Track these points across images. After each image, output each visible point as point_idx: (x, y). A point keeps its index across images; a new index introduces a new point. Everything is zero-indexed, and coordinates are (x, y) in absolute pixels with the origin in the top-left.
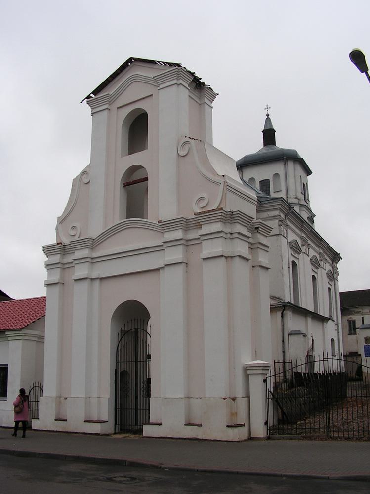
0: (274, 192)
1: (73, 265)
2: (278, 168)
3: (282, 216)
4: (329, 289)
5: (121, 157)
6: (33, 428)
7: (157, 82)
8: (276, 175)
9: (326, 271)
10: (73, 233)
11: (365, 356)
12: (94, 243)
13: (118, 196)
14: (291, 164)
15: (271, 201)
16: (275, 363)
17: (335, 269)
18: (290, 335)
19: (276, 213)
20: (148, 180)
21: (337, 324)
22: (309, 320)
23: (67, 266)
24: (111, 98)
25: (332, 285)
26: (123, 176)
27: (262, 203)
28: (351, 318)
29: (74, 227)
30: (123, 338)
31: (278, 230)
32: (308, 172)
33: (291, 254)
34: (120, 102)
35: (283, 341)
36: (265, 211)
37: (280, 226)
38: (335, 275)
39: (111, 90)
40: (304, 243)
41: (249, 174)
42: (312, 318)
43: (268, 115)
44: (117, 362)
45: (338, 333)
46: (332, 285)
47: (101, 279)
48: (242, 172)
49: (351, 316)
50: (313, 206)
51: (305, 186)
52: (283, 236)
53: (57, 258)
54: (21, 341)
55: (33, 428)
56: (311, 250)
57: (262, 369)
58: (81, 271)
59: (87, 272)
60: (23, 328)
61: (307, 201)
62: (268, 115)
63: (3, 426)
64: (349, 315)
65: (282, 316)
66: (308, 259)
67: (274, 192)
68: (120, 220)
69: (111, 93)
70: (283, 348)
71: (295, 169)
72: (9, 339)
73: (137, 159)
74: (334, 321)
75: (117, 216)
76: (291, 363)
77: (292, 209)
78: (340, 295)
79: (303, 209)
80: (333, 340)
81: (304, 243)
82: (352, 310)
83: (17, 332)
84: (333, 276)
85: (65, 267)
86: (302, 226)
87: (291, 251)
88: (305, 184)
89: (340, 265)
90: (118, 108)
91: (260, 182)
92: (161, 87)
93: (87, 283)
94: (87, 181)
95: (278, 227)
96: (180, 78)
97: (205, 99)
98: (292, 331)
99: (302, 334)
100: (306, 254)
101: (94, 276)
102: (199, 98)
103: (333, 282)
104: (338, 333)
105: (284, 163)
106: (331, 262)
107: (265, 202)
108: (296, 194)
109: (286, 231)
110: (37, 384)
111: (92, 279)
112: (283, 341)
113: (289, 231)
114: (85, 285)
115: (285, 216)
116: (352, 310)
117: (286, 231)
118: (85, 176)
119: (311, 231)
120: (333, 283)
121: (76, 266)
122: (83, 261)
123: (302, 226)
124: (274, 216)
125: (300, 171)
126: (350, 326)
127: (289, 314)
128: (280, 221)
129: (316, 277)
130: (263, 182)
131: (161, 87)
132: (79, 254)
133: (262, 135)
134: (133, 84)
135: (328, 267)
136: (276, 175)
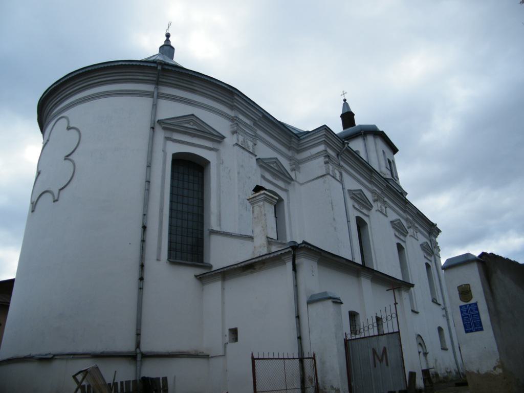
9: (409, 234)
11: (467, 332)
14: (370, 139)
16: (253, 359)
17: (433, 242)
18: (310, 302)
19: (322, 148)
21: (444, 308)
25: (431, 261)
27: (301, 138)
32: (394, 150)
33: (354, 206)
35: (298, 317)
37: (326, 163)
38: (435, 251)
40: (376, 198)
43: (345, 100)
45: (448, 320)
46: (431, 261)
52: (333, 177)
56: (388, 209)
62: (345, 100)
65: (295, 269)
66: (386, 222)
74: (439, 305)
77: (346, 146)
80: (440, 330)
84: (431, 250)
86: (371, 177)
99: (330, 298)
103: (433, 257)
104: (448, 320)
106: (427, 235)
112: (298, 317)
113: (344, 174)
119: (387, 186)
120: (432, 259)
124: (317, 153)
127: (307, 265)
129: (404, 247)
133: (340, 120)
135: (422, 239)
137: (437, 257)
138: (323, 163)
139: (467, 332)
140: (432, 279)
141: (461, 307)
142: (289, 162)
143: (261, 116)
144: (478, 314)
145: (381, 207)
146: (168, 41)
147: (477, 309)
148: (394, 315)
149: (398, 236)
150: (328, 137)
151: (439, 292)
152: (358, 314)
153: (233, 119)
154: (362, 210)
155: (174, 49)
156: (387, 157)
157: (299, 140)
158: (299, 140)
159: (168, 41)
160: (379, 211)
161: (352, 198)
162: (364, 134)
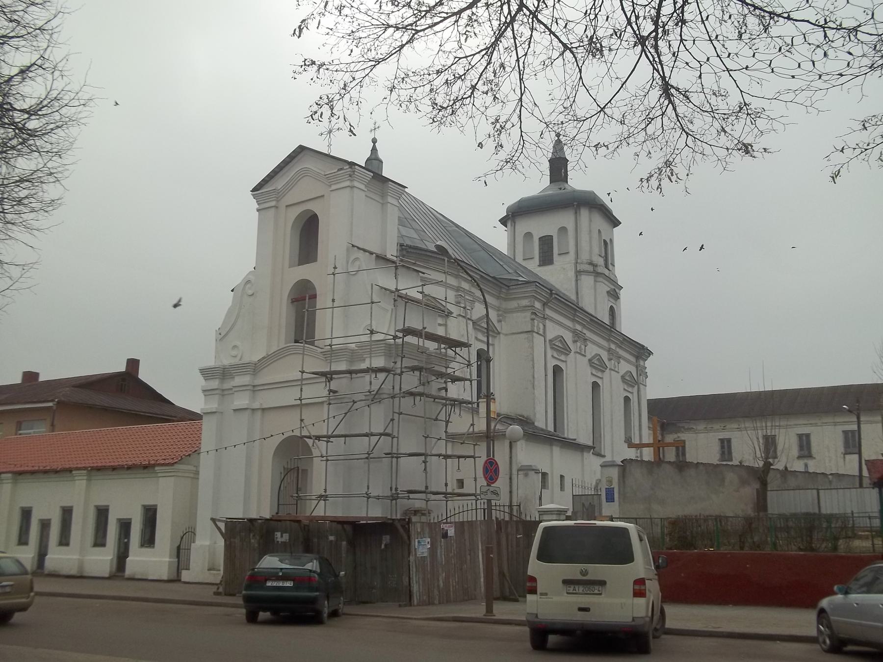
0: (559, 254)
1: (231, 392)
2: (566, 219)
3: (538, 305)
4: (627, 400)
5: (289, 268)
6: (183, 580)
7: (329, 180)
8: (563, 230)
10: (234, 353)
11: (607, 502)
12: (255, 368)
13: (284, 312)
14: (584, 213)
15: (522, 286)
20: (316, 298)
22: (556, 450)
23: (226, 392)
24: (278, 193)
26: (291, 290)
28: (679, 437)
29: (235, 347)
30: (286, 476)
31: (530, 325)
32: (615, 222)
34: (291, 198)
36: (514, 299)
37: (533, 319)
39: (279, 183)
41: (524, 226)
42: (561, 447)
44: (278, 505)
47: (263, 410)
48: (515, 223)
49: (679, 435)
50: (622, 270)
51: (607, 246)
53: (215, 384)
54: (173, 478)
55: (183, 580)
57: (557, 514)
58: (242, 400)
59: (247, 402)
60: (176, 463)
61: (610, 267)
63: (149, 578)
64: (676, 433)
67: (559, 254)
68: (286, 344)
69: (279, 188)
70: (511, 486)
71: (590, 221)
72: (160, 475)
73: (305, 272)
75: (281, 339)
76: (296, 506)
78: (648, 404)
79: (601, 279)
81: (576, 338)
82: (681, 425)
83: (167, 468)
84: (635, 381)
85: (223, 393)
86: (575, 315)
87: (550, 352)
88: (608, 241)
89: (650, 364)
90: (287, 206)
91: (540, 238)
92: (334, 187)
93: (247, 414)
94: (250, 292)
95: (530, 321)
96: (354, 180)
97: (389, 197)
98: (522, 466)
99: (533, 470)
100: (579, 353)
101: (256, 405)
102: (382, 196)
105: (574, 211)
106: (633, 359)
107: (514, 287)
108: (591, 256)
109: (544, 326)
110: (190, 529)
111: (253, 410)
114: (245, 417)
115: (544, 305)
116: (681, 425)
117: (544, 326)
118: (248, 286)
119: (591, 320)
121: (236, 393)
122: (244, 388)
123: (575, 315)
125: (599, 222)
126: (722, 447)
128: (533, 313)
130: (547, 238)
131: (334, 187)
132: (239, 380)
134: (305, 178)
135: (625, 367)
136: (563, 230)
137: (641, 386)
138: (528, 319)
139: (607, 502)
140: (630, 413)
141: (606, 488)
142: (496, 313)
143: (479, 277)
144: (614, 494)
145: (580, 347)
146: (374, 150)
147: (613, 491)
148: (574, 485)
149: (595, 374)
150: (537, 292)
151: (637, 428)
152: (548, 474)
153: (458, 289)
154: (560, 358)
155: (382, 162)
156: (603, 238)
157: (508, 290)
158: (508, 290)
159: (374, 150)
160: (577, 352)
161: (552, 348)
162: (577, 205)
